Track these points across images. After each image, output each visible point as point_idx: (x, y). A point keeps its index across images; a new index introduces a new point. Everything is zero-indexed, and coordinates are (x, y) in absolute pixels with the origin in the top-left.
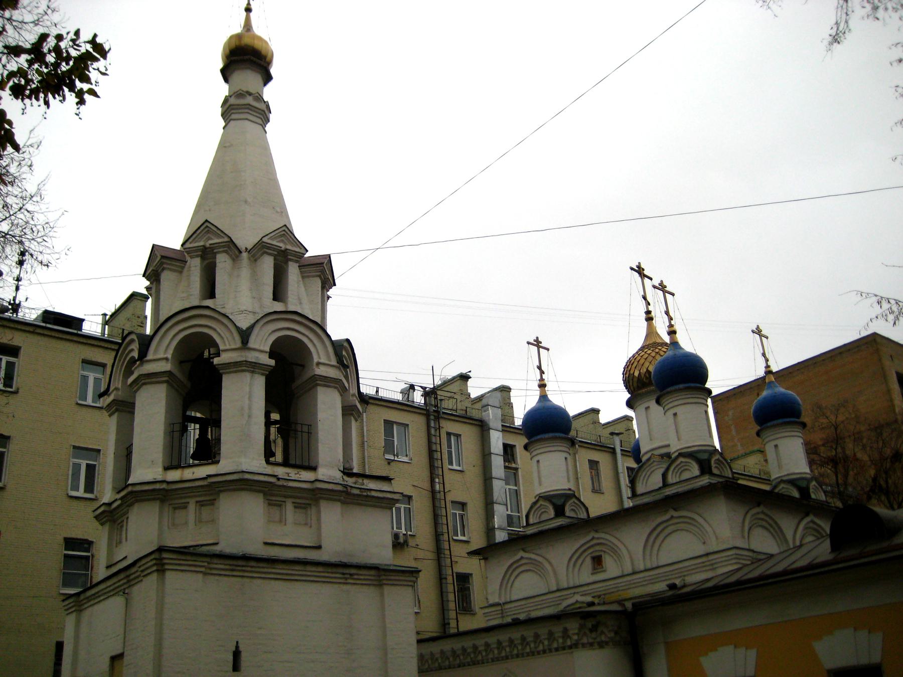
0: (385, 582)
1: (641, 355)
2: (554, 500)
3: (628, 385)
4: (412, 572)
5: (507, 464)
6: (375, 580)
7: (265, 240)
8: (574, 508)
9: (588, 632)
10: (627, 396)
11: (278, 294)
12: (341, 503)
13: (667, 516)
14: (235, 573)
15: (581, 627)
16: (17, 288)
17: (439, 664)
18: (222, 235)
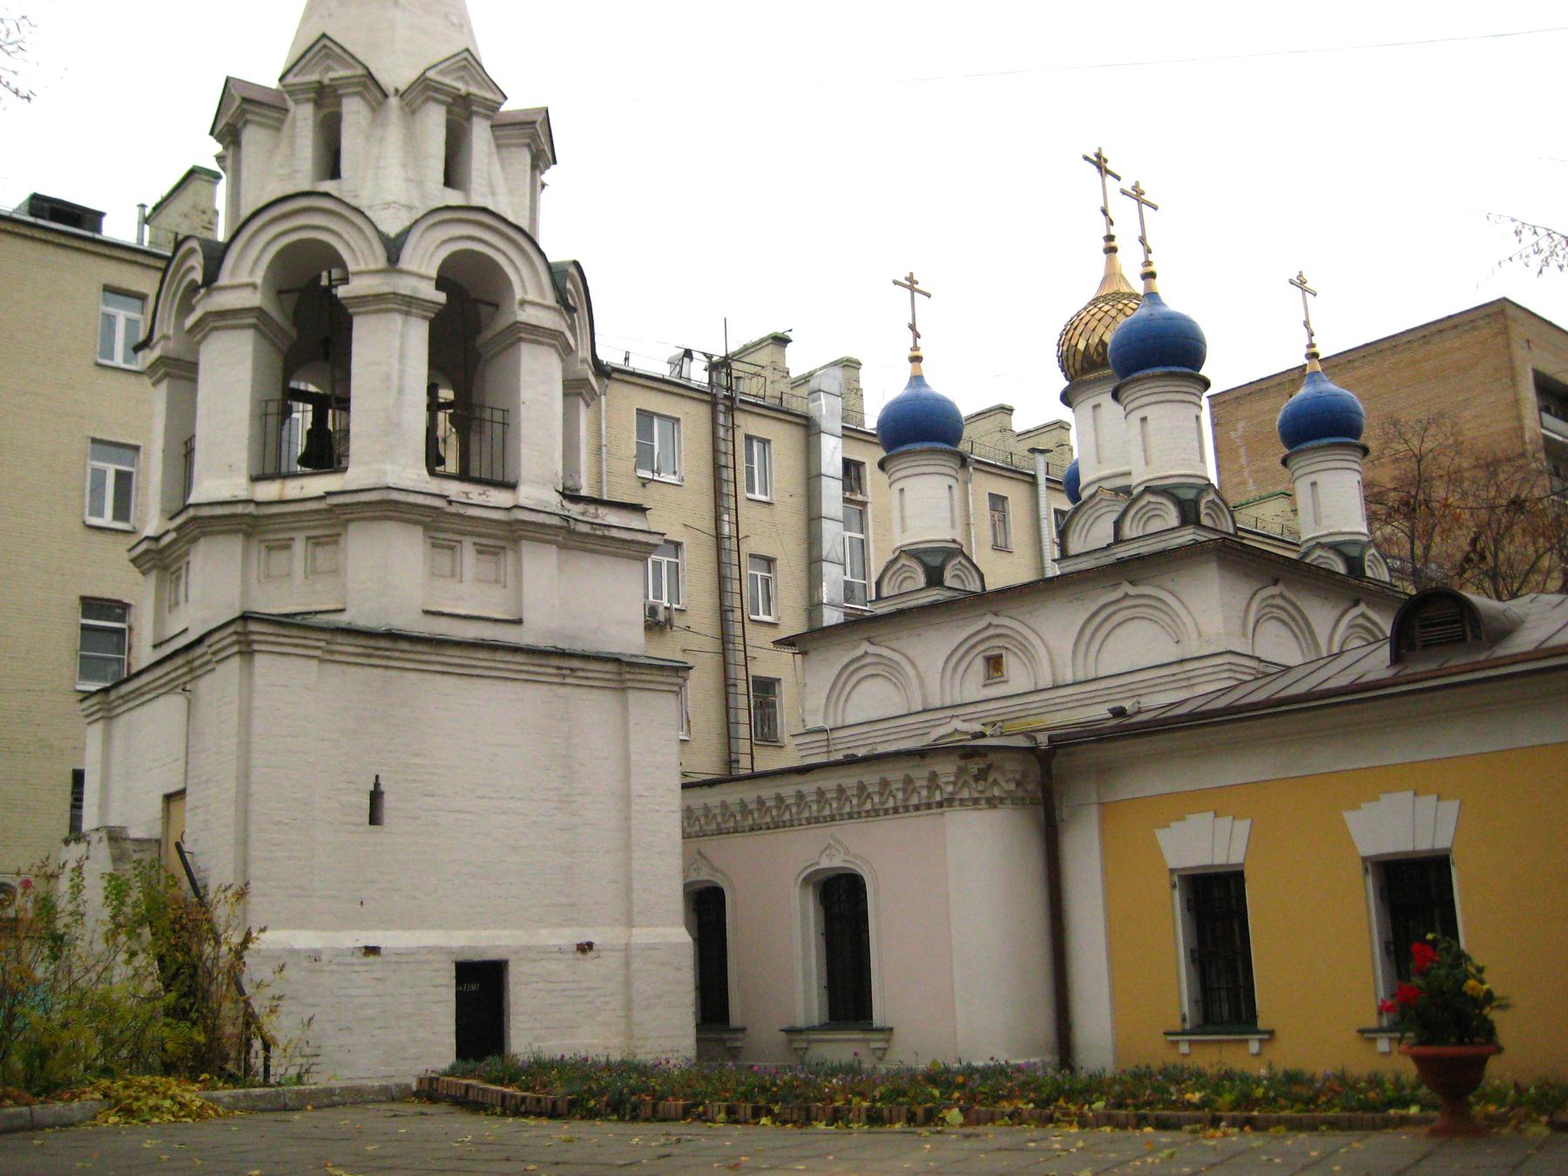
5: (848, 495)
8: (959, 573)
11: (453, 175)
15: (961, 771)
17: (718, 824)
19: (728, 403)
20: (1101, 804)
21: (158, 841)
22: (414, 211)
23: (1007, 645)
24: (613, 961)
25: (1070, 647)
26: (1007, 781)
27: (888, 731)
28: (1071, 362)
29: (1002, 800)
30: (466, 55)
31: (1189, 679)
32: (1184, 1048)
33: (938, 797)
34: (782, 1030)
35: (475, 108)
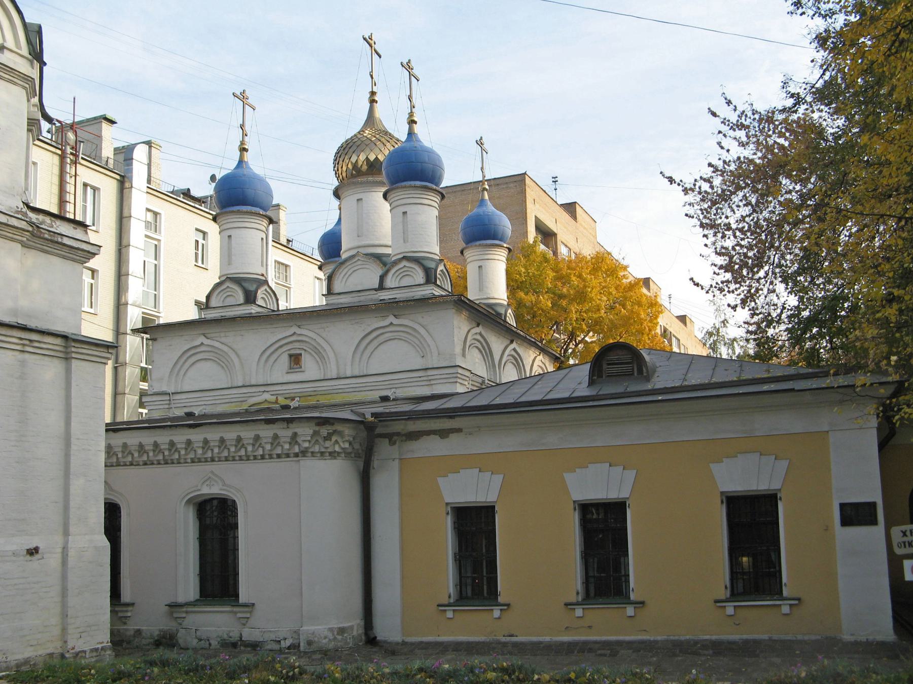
0: (74, 355)
1: (354, 141)
2: (246, 285)
6: (61, 352)
9: (321, 441)
10: (336, 183)
12: (22, 246)
13: (387, 322)
15: (316, 433)
19: (72, 157)
20: (400, 459)
23: (305, 348)
24: (53, 561)
25: (351, 354)
26: (343, 442)
27: (217, 398)
31: (430, 380)
32: (450, 614)
33: (296, 449)
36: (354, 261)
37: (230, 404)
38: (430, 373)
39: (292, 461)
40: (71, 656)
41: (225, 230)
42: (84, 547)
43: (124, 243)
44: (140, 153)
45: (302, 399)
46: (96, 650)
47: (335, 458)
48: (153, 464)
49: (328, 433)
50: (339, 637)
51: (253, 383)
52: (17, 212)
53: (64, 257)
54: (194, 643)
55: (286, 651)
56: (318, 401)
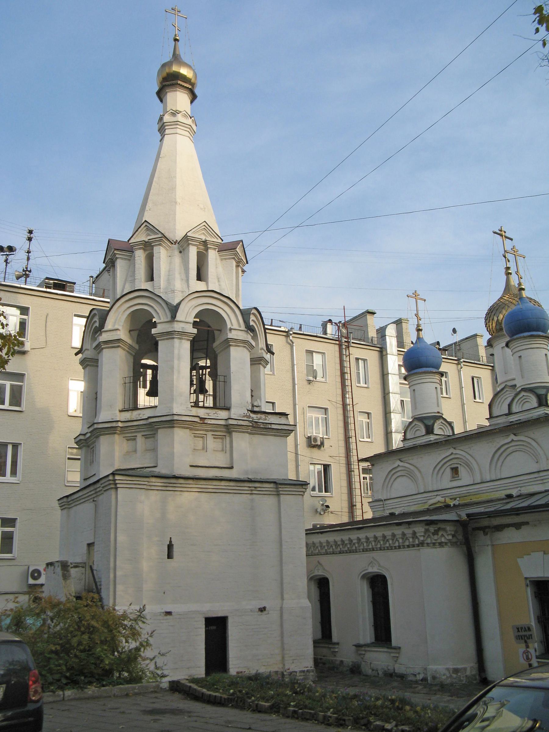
2: (426, 422)
3: (489, 328)
4: (302, 485)
7: (188, 234)
13: (509, 440)
14: (168, 489)
15: (427, 531)
16: (28, 259)
17: (326, 550)
18: (156, 231)
19: (346, 344)
21: (85, 563)
22: (185, 293)
23: (460, 463)
24: (274, 615)
26: (448, 535)
27: (410, 501)
28: (491, 327)
29: (446, 543)
30: (204, 224)
31: (542, 480)
34: (353, 645)
35: (209, 246)
36: (503, 392)
37: (418, 505)
38: (542, 474)
39: (416, 549)
40: (287, 674)
41: (412, 385)
42: (293, 607)
43: (386, 392)
44: (391, 331)
45: (462, 499)
46: (303, 671)
47: (443, 546)
48: (343, 553)
49: (434, 530)
50: (454, 676)
51: (431, 490)
52: (244, 417)
53: (275, 435)
54: (370, 672)
55: (420, 682)
56: (471, 499)
